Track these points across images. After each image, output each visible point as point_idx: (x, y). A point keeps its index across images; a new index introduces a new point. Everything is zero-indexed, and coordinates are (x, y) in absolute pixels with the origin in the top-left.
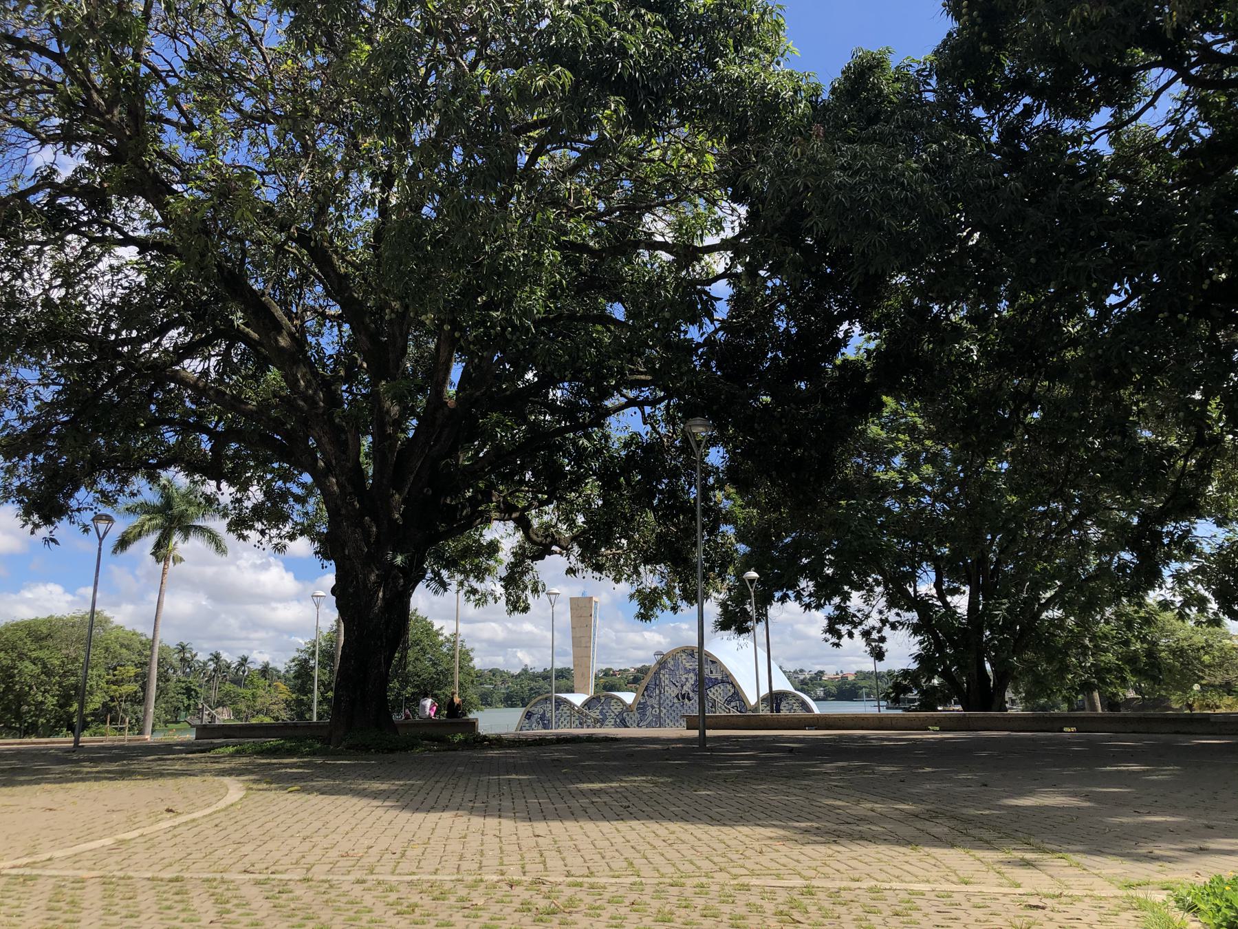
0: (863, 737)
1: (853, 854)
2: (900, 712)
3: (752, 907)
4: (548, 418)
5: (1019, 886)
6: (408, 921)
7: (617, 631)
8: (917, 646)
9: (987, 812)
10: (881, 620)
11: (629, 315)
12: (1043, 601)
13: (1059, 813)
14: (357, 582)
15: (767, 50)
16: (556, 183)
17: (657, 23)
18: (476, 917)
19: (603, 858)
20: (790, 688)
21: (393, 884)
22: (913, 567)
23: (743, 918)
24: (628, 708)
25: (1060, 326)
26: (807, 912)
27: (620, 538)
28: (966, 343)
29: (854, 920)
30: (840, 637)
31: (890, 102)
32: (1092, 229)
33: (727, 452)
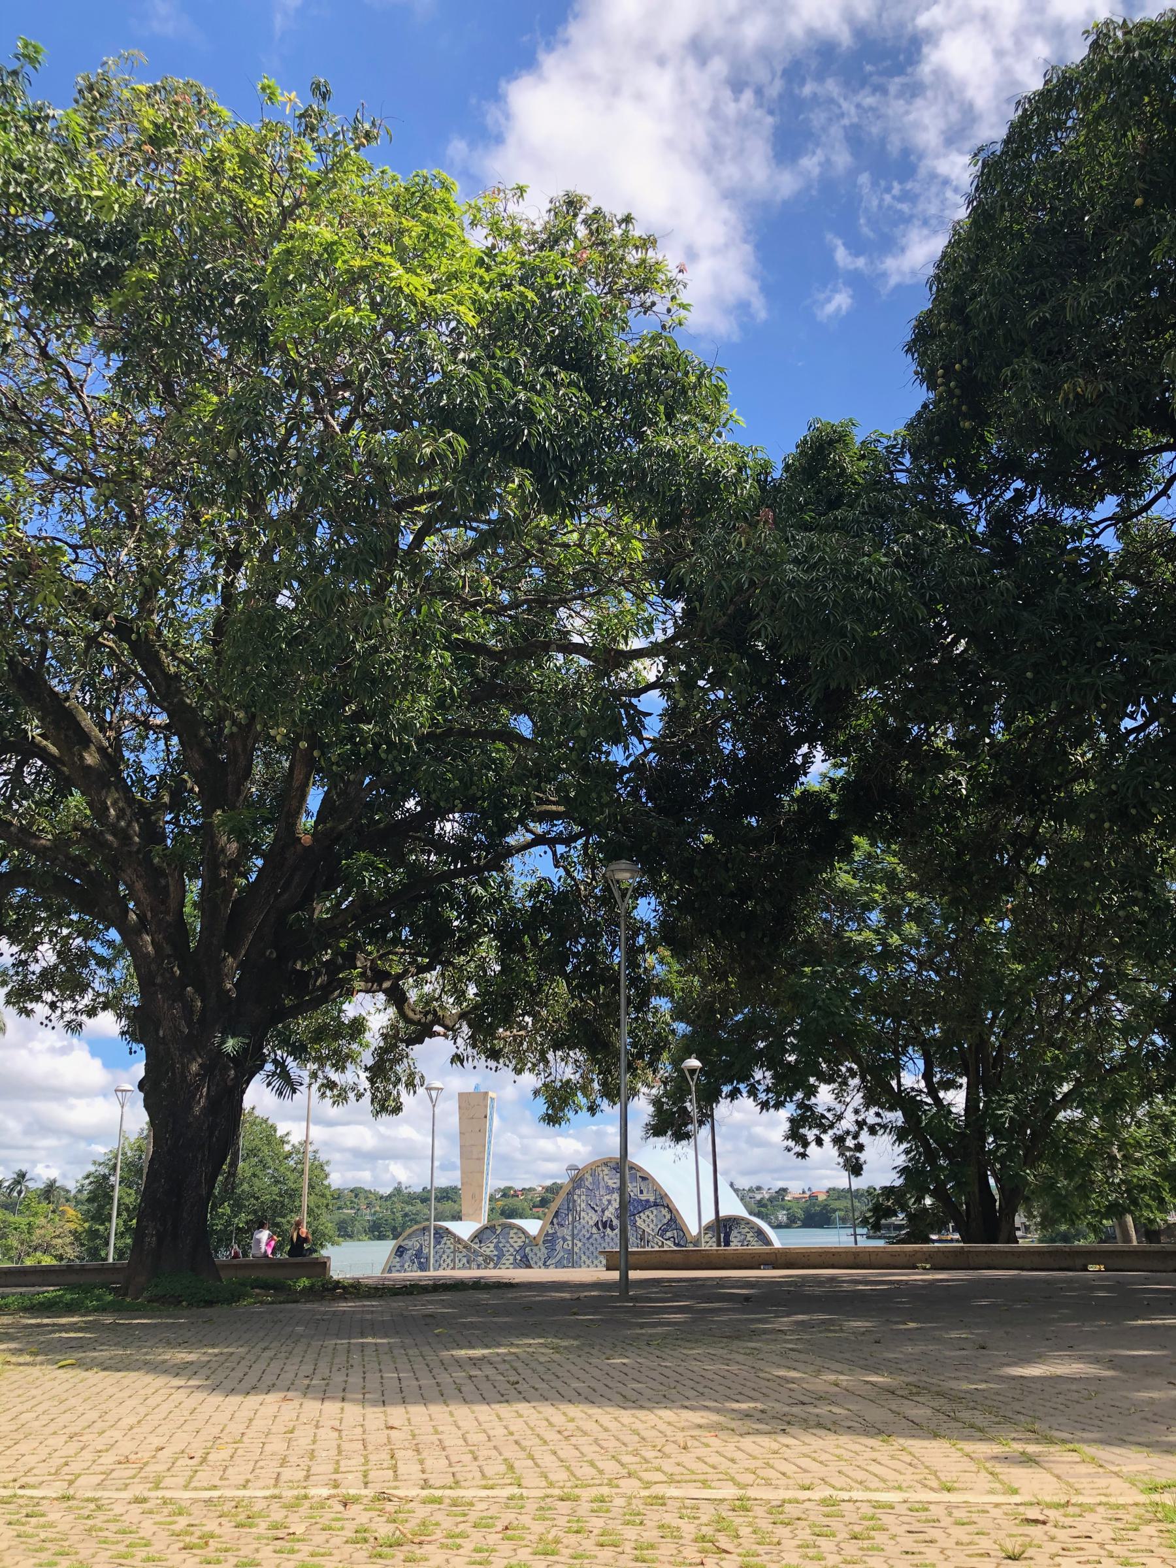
0: (832, 1279)
1: (805, 1449)
2: (880, 1243)
3: (668, 1532)
4: (433, 858)
5: (1015, 1492)
6: (197, 1559)
7: (521, 1137)
8: (903, 1157)
9: (983, 1386)
10: (857, 1122)
11: (537, 731)
12: (1059, 1097)
13: (1074, 1387)
14: (174, 1073)
15: (705, 419)
16: (448, 568)
17: (571, 384)
18: (292, 1551)
19: (475, 1459)
20: (743, 1213)
21: (183, 1504)
22: (895, 1052)
23: (652, 1547)
24: (532, 1241)
25: (1066, 754)
26: (738, 1537)
27: (523, 1015)
28: (952, 774)
29: (799, 1547)
30: (806, 1144)
31: (855, 483)
32: (1098, 639)
33: (661, 904)
